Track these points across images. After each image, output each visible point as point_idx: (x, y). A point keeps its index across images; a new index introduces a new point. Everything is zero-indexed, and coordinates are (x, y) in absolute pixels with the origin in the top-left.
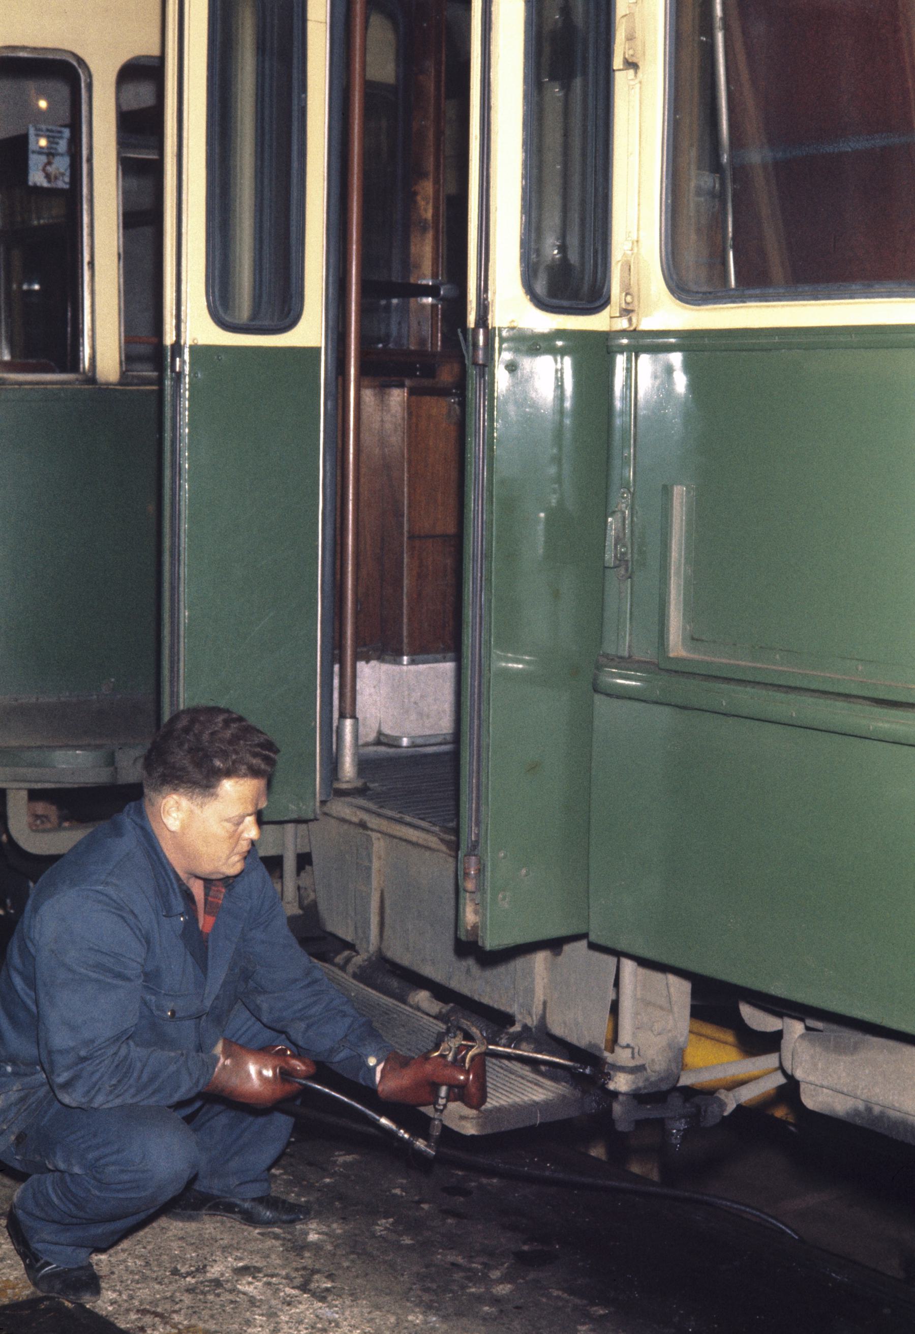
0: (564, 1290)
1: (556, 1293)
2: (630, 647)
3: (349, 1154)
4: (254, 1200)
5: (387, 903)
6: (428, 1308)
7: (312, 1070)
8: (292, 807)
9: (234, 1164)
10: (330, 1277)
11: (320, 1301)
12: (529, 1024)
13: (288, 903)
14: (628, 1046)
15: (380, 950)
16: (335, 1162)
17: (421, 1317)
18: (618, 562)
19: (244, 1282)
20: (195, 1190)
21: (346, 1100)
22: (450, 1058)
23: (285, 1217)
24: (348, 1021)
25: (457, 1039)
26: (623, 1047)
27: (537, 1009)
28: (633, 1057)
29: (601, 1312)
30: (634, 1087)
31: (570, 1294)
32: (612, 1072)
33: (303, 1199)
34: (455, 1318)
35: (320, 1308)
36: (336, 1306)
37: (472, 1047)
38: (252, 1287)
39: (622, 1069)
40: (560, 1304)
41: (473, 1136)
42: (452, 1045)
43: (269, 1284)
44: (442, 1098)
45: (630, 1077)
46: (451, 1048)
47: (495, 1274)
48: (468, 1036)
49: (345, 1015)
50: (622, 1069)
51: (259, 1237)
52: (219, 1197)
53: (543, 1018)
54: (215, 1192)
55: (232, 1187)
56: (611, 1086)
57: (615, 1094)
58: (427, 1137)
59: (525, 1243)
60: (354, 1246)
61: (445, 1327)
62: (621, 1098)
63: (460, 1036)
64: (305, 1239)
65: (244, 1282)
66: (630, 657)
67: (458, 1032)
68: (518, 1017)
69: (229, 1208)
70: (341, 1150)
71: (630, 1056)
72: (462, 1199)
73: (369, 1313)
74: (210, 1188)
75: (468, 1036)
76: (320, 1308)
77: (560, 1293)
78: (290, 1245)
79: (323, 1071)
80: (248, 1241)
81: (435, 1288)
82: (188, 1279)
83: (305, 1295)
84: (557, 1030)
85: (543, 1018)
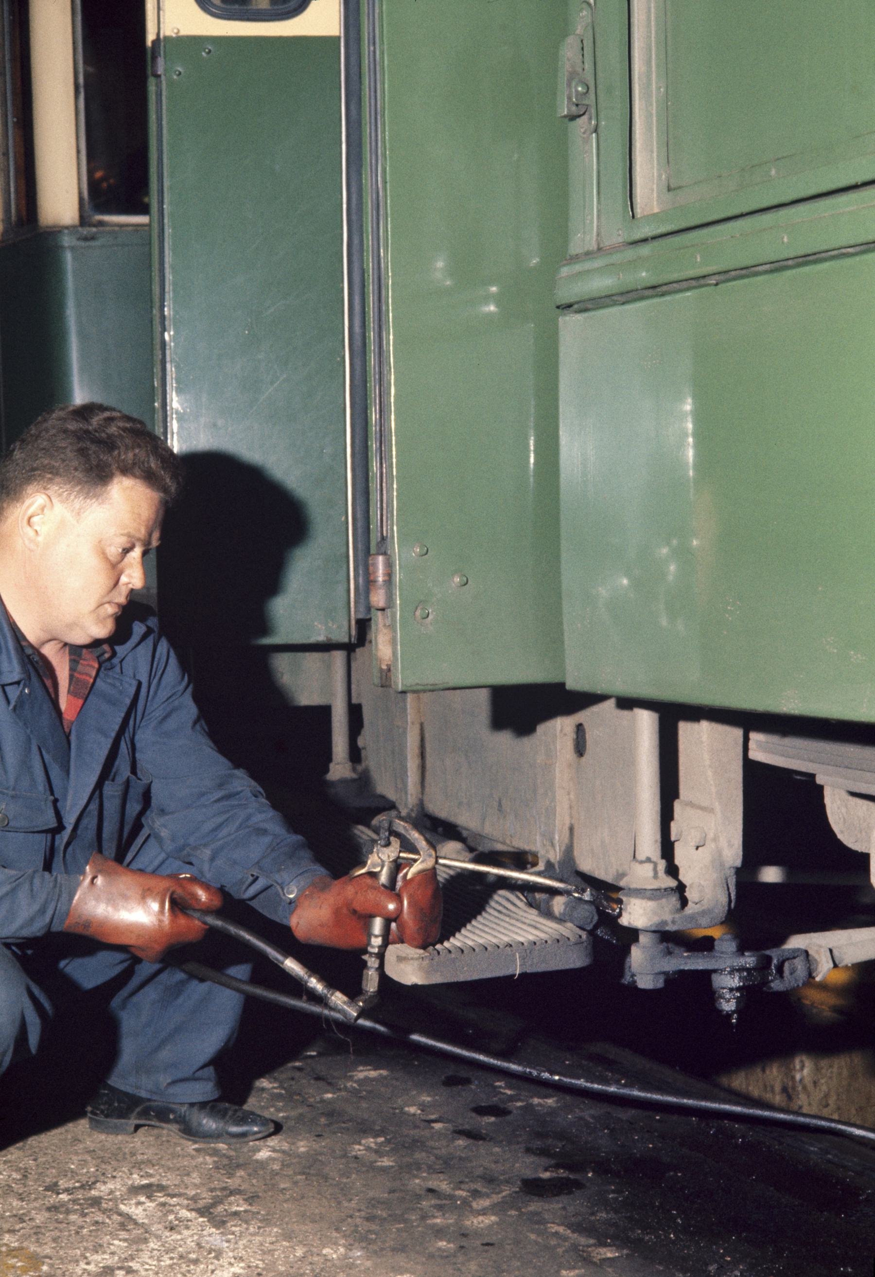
0: (569, 1226)
1: (554, 1228)
2: (598, 235)
3: (375, 1070)
4: (192, 1105)
5: (427, 736)
6: (360, 1238)
7: (217, 902)
8: (318, 626)
9: (165, 1054)
10: (252, 1199)
11: (215, 1226)
12: (552, 860)
13: (338, 764)
14: (648, 860)
15: (421, 804)
16: (352, 1077)
17: (342, 1250)
18: (574, 108)
19: (134, 1201)
20: (113, 1090)
21: (248, 937)
22: (383, 878)
23: (234, 1129)
24: (267, 840)
25: (391, 848)
26: (641, 862)
27: (560, 838)
28: (656, 876)
29: (609, 1255)
30: (656, 919)
31: (573, 1232)
32: (624, 899)
33: (281, 1115)
34: (390, 1254)
35: (210, 1235)
36: (233, 1233)
37: (415, 861)
38: (140, 1208)
39: (639, 893)
40: (553, 1242)
41: (415, 987)
42: (384, 857)
43: (163, 1204)
44: (376, 936)
45: (650, 904)
46: (383, 861)
47: (479, 1204)
48: (408, 846)
49: (264, 832)
50: (639, 893)
51: (194, 1153)
52: (149, 1100)
53: (569, 851)
54: (143, 1094)
55: (162, 1088)
56: (624, 921)
57: (632, 934)
58: (353, 991)
59: (546, 1170)
60: (310, 1168)
61: (369, 1264)
62: (643, 939)
63: (395, 843)
64: (251, 1157)
65: (134, 1201)
66: (599, 249)
67: (392, 839)
68: (541, 853)
69: (163, 1115)
70: (370, 1065)
71: (651, 874)
72: (493, 1119)
73: (272, 1243)
74: (138, 1087)
75: (408, 846)
76: (210, 1235)
77: (561, 1229)
78: (225, 1161)
79: (232, 907)
80: (174, 1156)
81: (387, 1222)
82: (61, 1196)
83: (201, 1220)
84: (586, 865)
85: (569, 851)
